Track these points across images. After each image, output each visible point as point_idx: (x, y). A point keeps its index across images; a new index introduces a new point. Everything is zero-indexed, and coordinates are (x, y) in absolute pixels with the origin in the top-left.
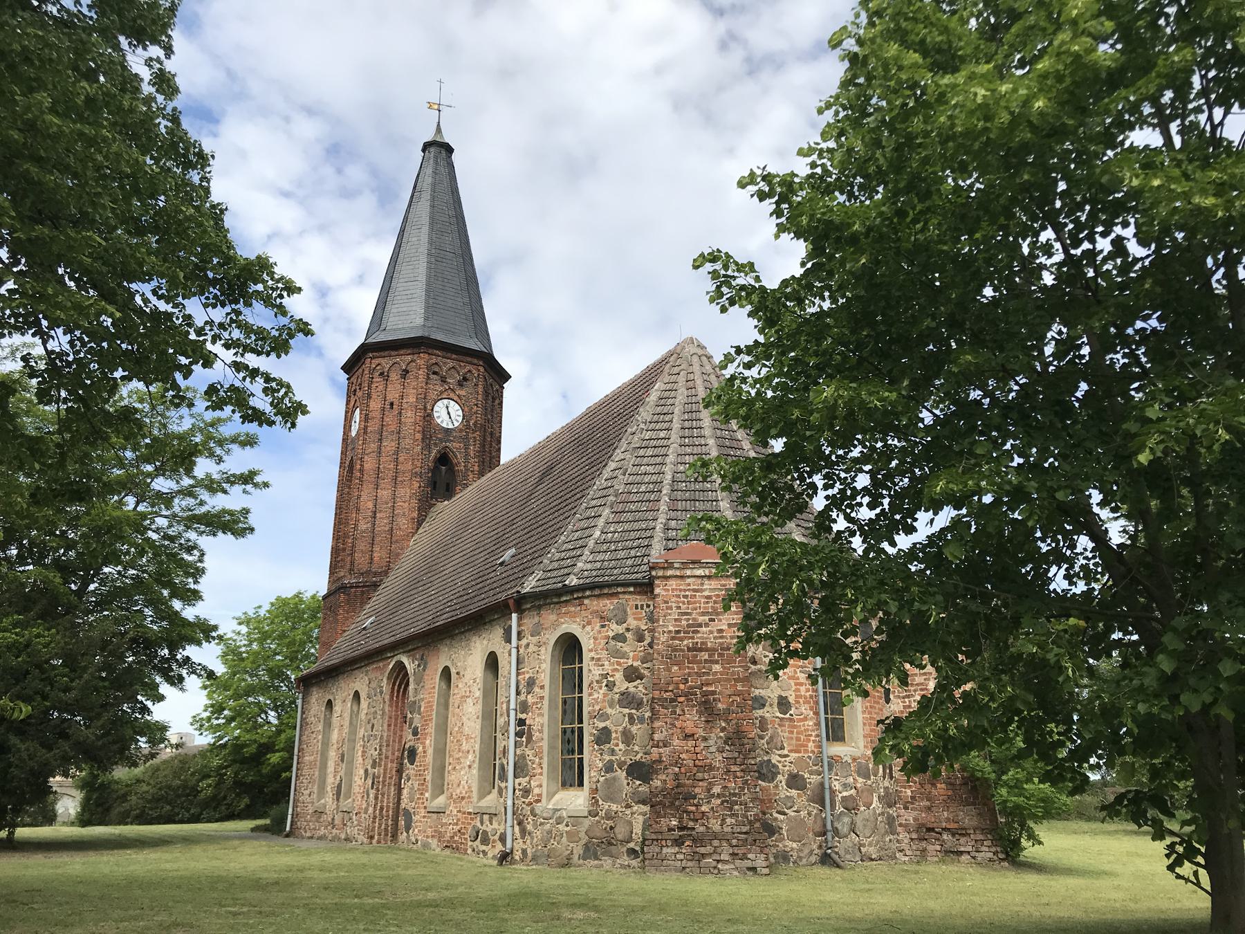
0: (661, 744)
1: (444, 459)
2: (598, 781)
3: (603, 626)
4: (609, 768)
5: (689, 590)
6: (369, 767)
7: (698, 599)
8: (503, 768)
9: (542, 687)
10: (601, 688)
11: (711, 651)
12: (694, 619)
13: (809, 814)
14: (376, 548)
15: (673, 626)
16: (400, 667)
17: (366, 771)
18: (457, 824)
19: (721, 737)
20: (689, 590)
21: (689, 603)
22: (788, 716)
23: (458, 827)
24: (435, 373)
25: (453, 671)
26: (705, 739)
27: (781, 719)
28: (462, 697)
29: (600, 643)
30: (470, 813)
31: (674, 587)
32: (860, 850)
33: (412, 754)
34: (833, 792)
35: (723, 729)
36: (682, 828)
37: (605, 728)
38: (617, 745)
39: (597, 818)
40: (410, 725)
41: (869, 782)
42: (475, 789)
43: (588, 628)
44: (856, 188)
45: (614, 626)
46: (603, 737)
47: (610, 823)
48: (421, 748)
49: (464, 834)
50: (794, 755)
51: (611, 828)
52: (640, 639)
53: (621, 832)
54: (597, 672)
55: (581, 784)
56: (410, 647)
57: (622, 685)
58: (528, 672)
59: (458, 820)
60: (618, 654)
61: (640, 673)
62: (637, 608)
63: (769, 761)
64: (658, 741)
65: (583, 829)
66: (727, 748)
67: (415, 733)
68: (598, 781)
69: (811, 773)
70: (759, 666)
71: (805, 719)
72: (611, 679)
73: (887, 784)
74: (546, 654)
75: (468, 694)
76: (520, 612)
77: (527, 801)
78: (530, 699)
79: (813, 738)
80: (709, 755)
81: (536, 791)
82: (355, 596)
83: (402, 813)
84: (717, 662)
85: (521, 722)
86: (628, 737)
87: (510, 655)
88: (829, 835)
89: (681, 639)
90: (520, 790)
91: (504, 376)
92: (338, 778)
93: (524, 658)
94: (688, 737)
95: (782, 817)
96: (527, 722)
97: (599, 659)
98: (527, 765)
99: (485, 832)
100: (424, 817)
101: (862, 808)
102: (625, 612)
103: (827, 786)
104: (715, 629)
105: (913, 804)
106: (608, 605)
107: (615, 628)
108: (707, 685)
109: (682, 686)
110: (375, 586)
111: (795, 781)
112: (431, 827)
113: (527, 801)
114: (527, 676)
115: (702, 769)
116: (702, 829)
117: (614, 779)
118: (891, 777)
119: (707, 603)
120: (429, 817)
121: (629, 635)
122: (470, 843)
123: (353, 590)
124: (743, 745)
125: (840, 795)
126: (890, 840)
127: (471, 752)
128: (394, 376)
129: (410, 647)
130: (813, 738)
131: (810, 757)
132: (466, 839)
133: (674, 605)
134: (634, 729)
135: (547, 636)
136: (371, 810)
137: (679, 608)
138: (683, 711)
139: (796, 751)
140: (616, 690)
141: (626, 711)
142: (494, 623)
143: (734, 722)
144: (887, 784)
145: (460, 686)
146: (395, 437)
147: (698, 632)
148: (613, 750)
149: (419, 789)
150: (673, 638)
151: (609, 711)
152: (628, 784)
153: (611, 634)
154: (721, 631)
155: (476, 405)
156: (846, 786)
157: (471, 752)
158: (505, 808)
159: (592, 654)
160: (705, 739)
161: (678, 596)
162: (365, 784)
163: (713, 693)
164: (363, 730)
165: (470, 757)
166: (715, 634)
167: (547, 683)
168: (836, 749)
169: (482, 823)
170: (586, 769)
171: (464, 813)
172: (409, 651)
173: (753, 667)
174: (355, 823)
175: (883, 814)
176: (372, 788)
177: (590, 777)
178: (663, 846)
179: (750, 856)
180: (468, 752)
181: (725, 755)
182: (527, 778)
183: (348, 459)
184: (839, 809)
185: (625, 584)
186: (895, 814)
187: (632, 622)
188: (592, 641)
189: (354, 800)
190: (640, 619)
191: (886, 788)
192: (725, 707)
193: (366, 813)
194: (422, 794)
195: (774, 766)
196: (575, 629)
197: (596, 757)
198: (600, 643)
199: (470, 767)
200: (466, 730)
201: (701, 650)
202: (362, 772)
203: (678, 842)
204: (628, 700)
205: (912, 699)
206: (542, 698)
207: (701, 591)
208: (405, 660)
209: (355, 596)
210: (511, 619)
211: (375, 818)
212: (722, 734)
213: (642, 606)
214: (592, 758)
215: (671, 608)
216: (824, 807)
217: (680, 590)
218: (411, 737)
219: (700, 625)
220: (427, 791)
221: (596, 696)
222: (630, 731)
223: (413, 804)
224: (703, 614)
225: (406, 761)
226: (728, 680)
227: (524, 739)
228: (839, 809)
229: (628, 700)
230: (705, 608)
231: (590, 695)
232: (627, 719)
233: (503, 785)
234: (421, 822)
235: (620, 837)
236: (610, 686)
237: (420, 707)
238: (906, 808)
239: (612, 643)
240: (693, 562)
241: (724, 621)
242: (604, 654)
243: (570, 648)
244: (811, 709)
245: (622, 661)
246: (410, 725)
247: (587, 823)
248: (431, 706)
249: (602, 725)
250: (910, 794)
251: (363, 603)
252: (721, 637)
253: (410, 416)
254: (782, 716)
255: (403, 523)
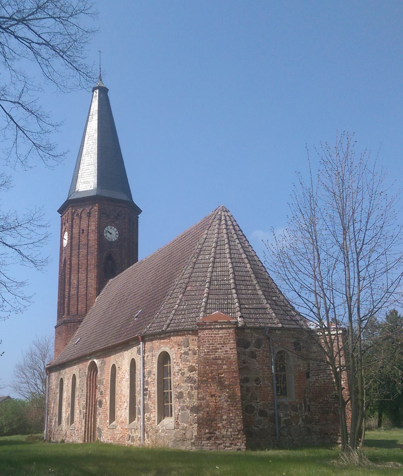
0: (201, 399)
1: (110, 257)
2: (178, 415)
3: (179, 348)
4: (182, 409)
5: (213, 334)
6: (82, 409)
7: (217, 338)
8: (139, 408)
9: (154, 374)
10: (179, 375)
11: (223, 360)
12: (215, 346)
13: (269, 427)
14: (80, 303)
15: (207, 350)
16: (93, 364)
17: (80, 411)
18: (121, 434)
19: (226, 396)
20: (213, 334)
21: (213, 339)
22: (259, 386)
23: (122, 435)
24: (104, 213)
25: (117, 366)
26: (220, 397)
27: (257, 387)
28: (121, 378)
29: (178, 356)
30: (126, 429)
31: (207, 333)
32: (292, 442)
33: (101, 403)
34: (279, 418)
35: (227, 392)
36: (210, 433)
37: (181, 392)
38: (186, 399)
39: (178, 430)
40: (99, 390)
41: (297, 413)
42: (128, 418)
43: (173, 349)
44: (98, 403)
45: (184, 348)
46: (180, 396)
47: (184, 432)
48: (104, 400)
49: (124, 438)
50: (262, 402)
51: (184, 434)
52: (195, 354)
53: (188, 435)
54: (177, 368)
55: (171, 416)
56: (98, 355)
57: (188, 374)
58: (148, 368)
59: (121, 432)
60: (187, 361)
61: (195, 368)
62: (193, 341)
63: (251, 405)
64: (200, 398)
65: (173, 434)
66: (229, 400)
67: (101, 394)
68: (178, 415)
69: (270, 409)
70: (246, 365)
71: (267, 386)
72: (182, 371)
73: (306, 414)
74: (155, 361)
75: (123, 377)
76: (144, 342)
77: (149, 423)
78: (149, 380)
79: (270, 395)
80: (221, 403)
81: (153, 419)
82: (71, 327)
83: (97, 429)
84: (225, 364)
85: (145, 390)
86: (190, 396)
87: (140, 360)
88: (277, 436)
89: (210, 355)
90: (146, 419)
91: (140, 211)
92: (68, 414)
93: (146, 362)
94: (212, 396)
95: (256, 428)
96: (149, 390)
97: (178, 363)
98: (149, 408)
99: (133, 437)
100: (107, 431)
101: (294, 424)
102: (188, 342)
103: (276, 415)
104: (224, 350)
105: (319, 422)
106: (180, 339)
107: (184, 349)
108: (222, 374)
109: (210, 375)
110: (80, 322)
111: (262, 413)
112: (110, 435)
113: (149, 423)
114: (148, 370)
115: (218, 409)
116: (218, 433)
117: (185, 413)
118: (309, 410)
119: (221, 339)
120: (109, 431)
121: (190, 352)
122: (126, 442)
123: (69, 324)
124: (236, 399)
125: (283, 419)
126: (308, 439)
127: (126, 402)
128: (84, 216)
129: (98, 355)
130: (270, 395)
131: (269, 403)
132: (125, 440)
133: (207, 340)
134: (193, 392)
135: (156, 352)
136: (83, 428)
137: (209, 342)
138: (211, 385)
139: (263, 401)
140: (185, 376)
141: (190, 385)
142: (133, 345)
143: (232, 389)
144: (306, 414)
145: (120, 373)
146: (86, 247)
147: (217, 352)
148: (184, 401)
149: (104, 419)
150: (206, 355)
151: (182, 385)
152: (191, 415)
153: (182, 352)
154: (227, 351)
155: (125, 228)
156: (286, 415)
157: (126, 402)
158: (141, 426)
159: (175, 360)
160: (220, 397)
161: (209, 337)
162: (80, 417)
163: (223, 377)
164: (78, 392)
165: (126, 404)
166: (224, 353)
167: (156, 373)
168: (284, 400)
169: (131, 433)
170: (173, 409)
171: (124, 429)
172: (97, 357)
173: (244, 365)
174: (77, 434)
175: (304, 427)
176: (83, 419)
177: (175, 413)
178: (202, 441)
179: (238, 444)
180: (125, 402)
181: (228, 403)
182: (149, 413)
183: (63, 258)
184: (283, 425)
185: (188, 330)
186: (311, 427)
187: (191, 347)
188: (174, 355)
189: (75, 424)
190: (195, 345)
191: (306, 416)
192: (228, 383)
193: (81, 430)
194: (105, 421)
195: (254, 407)
196: (167, 349)
197: (177, 404)
198: (178, 356)
199: (125, 409)
200: (124, 392)
201: (218, 359)
202: (78, 411)
203: (209, 439)
204: (190, 380)
205: (319, 376)
206: (154, 379)
207: (219, 334)
208: (96, 361)
209: (71, 327)
210: (140, 344)
211: (85, 432)
212: (227, 394)
213: (195, 339)
214: (176, 405)
215: (205, 342)
216: (275, 424)
217: (209, 334)
218: (99, 395)
219: (218, 349)
220: (107, 419)
221: (176, 378)
222: (191, 393)
223: (102, 425)
224: (219, 344)
225: (98, 406)
226: (229, 372)
227: (147, 397)
228: (283, 425)
229: (190, 380)
230: (220, 341)
231: (174, 378)
232: (190, 388)
233: (139, 416)
234: (106, 433)
235: (188, 437)
236: (183, 374)
237: (103, 382)
238: (316, 424)
239: (183, 355)
240: (215, 322)
241: (228, 347)
242: (179, 361)
243: (164, 358)
244: (270, 382)
245: (187, 363)
246: (99, 390)
247: (174, 432)
248: (108, 382)
249: (179, 391)
250: (317, 418)
251: (74, 332)
252: (227, 354)
253: (93, 237)
254: (257, 386)
255: (92, 290)
